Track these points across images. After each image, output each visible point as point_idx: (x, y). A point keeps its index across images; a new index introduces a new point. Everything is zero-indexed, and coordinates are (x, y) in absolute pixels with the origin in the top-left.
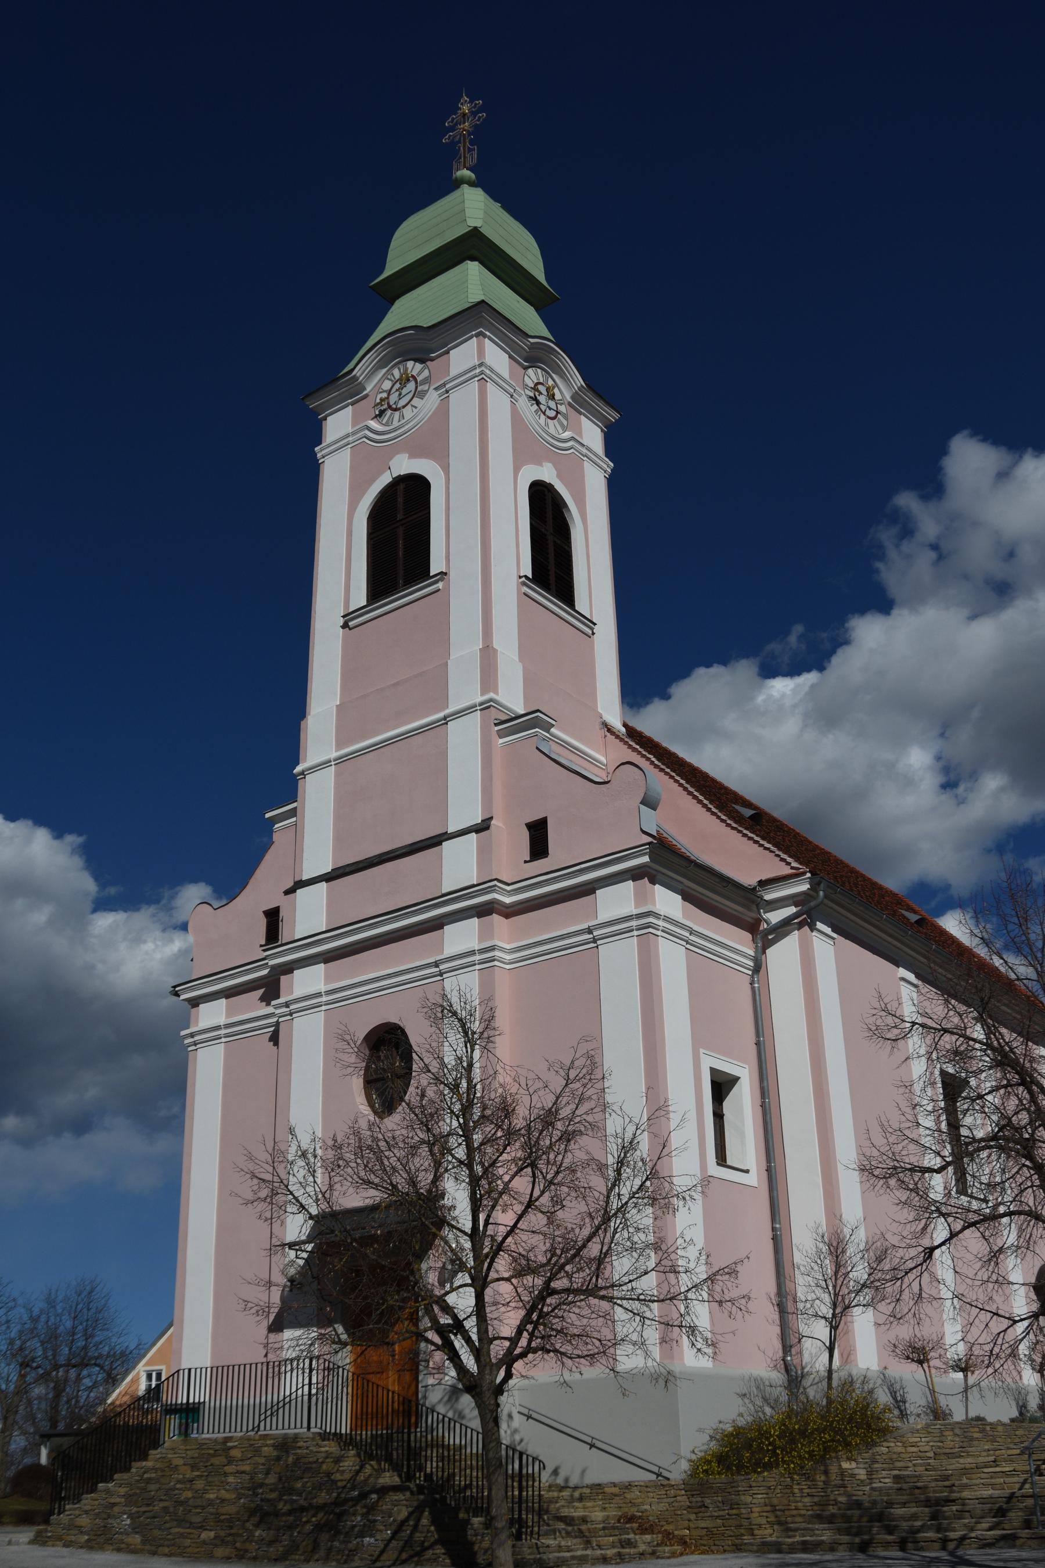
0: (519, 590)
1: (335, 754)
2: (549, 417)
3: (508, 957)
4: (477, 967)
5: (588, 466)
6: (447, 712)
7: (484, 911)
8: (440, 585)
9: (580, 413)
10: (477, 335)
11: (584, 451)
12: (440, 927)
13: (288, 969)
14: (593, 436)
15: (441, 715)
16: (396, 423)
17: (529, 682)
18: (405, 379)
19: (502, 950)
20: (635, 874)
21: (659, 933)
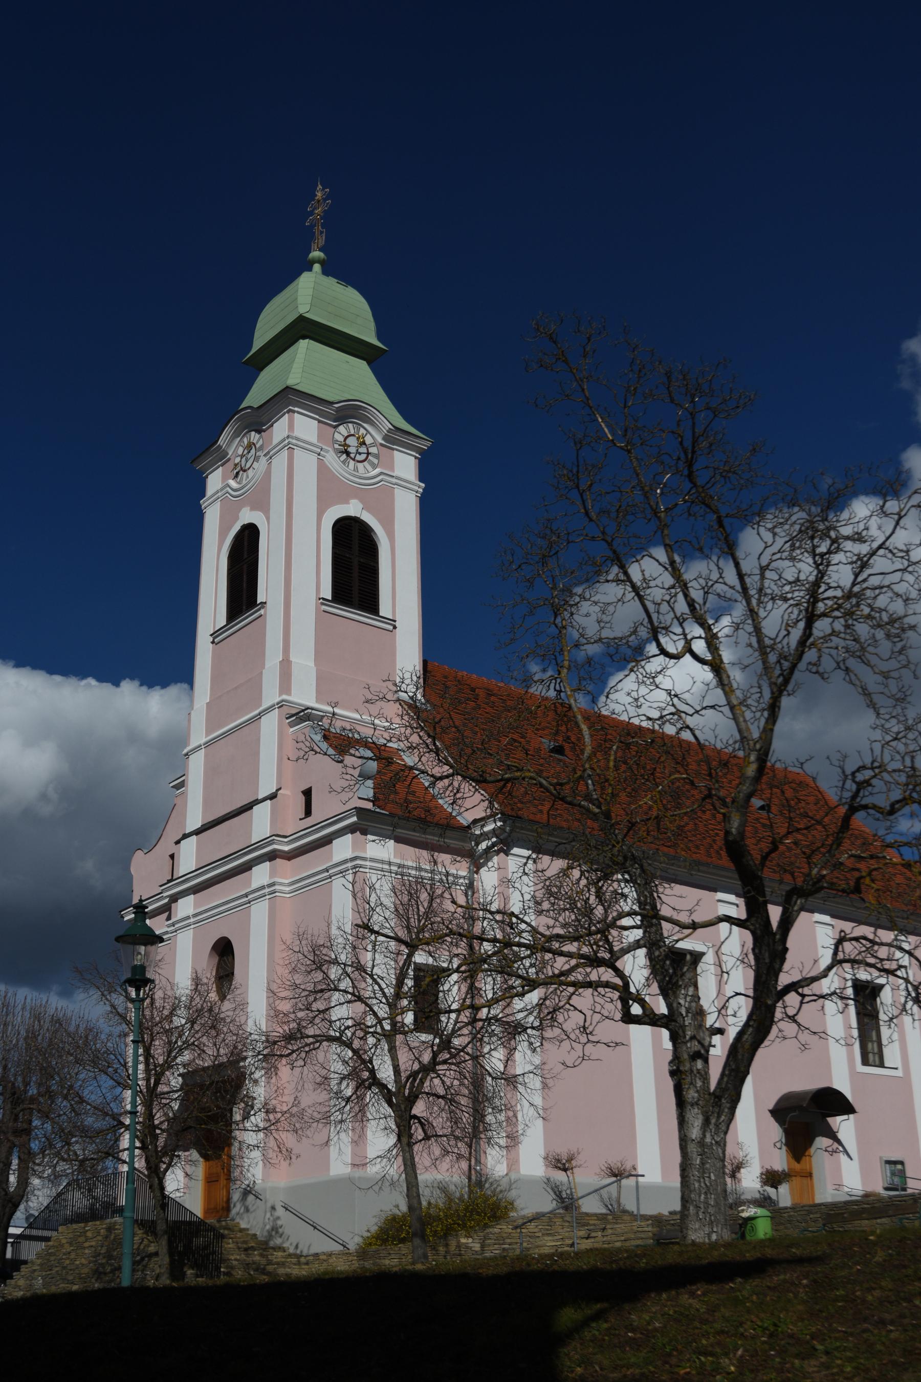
0: (317, 609)
1: (204, 740)
2: (359, 462)
3: (288, 889)
4: (268, 897)
5: (399, 493)
6: (261, 709)
7: (272, 856)
8: (262, 612)
9: (393, 449)
10: (288, 412)
11: (394, 480)
12: (250, 868)
13: (174, 899)
14: (405, 465)
15: (257, 712)
16: (244, 482)
17: (322, 681)
18: (250, 446)
19: (281, 884)
20: (351, 829)
21: (367, 870)
